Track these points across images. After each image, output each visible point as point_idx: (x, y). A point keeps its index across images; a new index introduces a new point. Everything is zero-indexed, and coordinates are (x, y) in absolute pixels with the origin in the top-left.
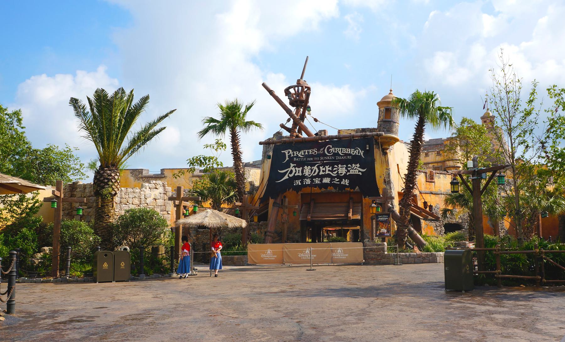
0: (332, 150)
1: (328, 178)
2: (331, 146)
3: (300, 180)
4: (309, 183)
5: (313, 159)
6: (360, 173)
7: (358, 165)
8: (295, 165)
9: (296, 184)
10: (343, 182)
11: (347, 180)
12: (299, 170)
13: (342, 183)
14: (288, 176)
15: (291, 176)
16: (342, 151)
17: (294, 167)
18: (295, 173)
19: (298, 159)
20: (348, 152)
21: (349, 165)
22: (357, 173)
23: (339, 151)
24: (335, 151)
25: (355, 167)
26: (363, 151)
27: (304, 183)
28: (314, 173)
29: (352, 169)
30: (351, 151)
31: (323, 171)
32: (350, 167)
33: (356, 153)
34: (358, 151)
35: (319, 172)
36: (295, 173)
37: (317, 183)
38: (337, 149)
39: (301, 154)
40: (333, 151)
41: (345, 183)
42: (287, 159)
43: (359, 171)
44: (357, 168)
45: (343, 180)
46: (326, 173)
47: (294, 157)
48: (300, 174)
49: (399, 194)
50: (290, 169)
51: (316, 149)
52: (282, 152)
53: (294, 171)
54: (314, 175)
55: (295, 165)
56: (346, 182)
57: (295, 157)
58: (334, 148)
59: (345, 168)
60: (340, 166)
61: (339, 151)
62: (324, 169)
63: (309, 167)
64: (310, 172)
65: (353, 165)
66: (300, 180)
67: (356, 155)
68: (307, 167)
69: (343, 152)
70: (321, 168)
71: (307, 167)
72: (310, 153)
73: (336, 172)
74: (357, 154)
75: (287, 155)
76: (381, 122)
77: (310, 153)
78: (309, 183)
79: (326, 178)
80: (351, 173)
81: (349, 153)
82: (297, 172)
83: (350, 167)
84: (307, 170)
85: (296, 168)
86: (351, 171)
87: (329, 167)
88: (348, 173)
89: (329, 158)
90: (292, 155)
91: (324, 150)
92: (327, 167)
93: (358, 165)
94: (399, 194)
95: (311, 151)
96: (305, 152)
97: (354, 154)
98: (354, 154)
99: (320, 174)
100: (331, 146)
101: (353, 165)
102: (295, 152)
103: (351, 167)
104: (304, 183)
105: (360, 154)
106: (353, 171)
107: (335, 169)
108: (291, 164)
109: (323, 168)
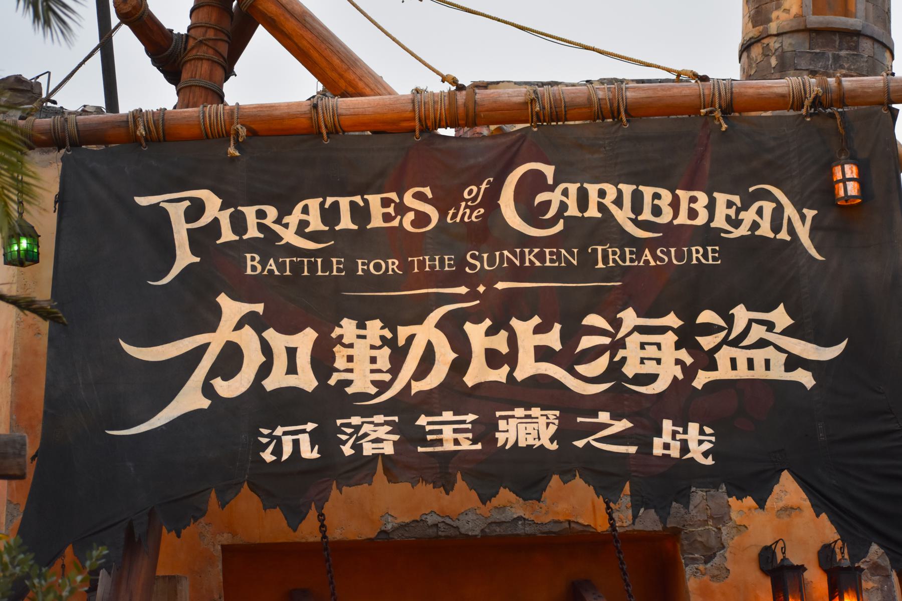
0: (555, 197)
1: (536, 412)
2: (549, 171)
3: (310, 426)
4: (388, 449)
5: (406, 266)
6: (805, 378)
7: (781, 317)
8: (259, 308)
9: (278, 451)
10: (666, 438)
11: (693, 427)
12: (292, 353)
13: (658, 451)
14: (208, 390)
15: (228, 389)
16: (637, 207)
17: (248, 320)
18: (265, 370)
19: (281, 266)
20: (693, 214)
21: (707, 316)
22: (778, 373)
23: (618, 202)
24: (583, 203)
25: (758, 332)
26: (810, 213)
27: (347, 450)
28: (422, 371)
29: (736, 343)
30: (711, 207)
31: (493, 359)
32: (709, 329)
33: (755, 226)
34: (768, 207)
35: (460, 366)
36: (265, 370)
37: (449, 446)
38: (602, 194)
39: (303, 224)
40: (563, 207)
41: (685, 448)
42: (185, 257)
43: (793, 362)
44: (770, 337)
45: (667, 425)
46: (520, 375)
47: (244, 246)
48: (306, 380)
49: (454, 415)
50: (216, 341)
51: (427, 191)
52: (143, 201)
53: (253, 359)
54: (417, 387)
55: (259, 308)
56: (692, 445)
57: (253, 245)
58: (573, 188)
59: (669, 339)
60: (629, 318)
61: (618, 202)
62: (500, 343)
63: (375, 328)
64: (384, 362)
65: (741, 314)
66: (310, 426)
67: (753, 242)
68: (361, 326)
69: (646, 215)
70: (475, 332)
71: (361, 326)
72: (376, 222)
73: (600, 365)
74: (765, 230)
75: (181, 230)
76: (788, 42)
77: (376, 222)
78: (388, 449)
79: (519, 412)
80: (724, 372)
81: (702, 219)
82: (280, 362)
83: (709, 329)
84: (361, 351)
85: (271, 334)
86: (723, 356)
87: (538, 330)
88: (702, 379)
89: (541, 257)
90: (227, 235)
91: (491, 199)
92: (524, 328)
93: (781, 317)
94: (454, 415)
95: (386, 203)
96: (330, 215)
97: (743, 231)
98: (737, 233)
99: (470, 379)
100: (549, 171)
101: (741, 314)
102: (250, 212)
103: (718, 329)
104: (347, 450)
105: (792, 231)
106: (741, 356)
107: (586, 342)
108: (223, 300)
109: (490, 332)
